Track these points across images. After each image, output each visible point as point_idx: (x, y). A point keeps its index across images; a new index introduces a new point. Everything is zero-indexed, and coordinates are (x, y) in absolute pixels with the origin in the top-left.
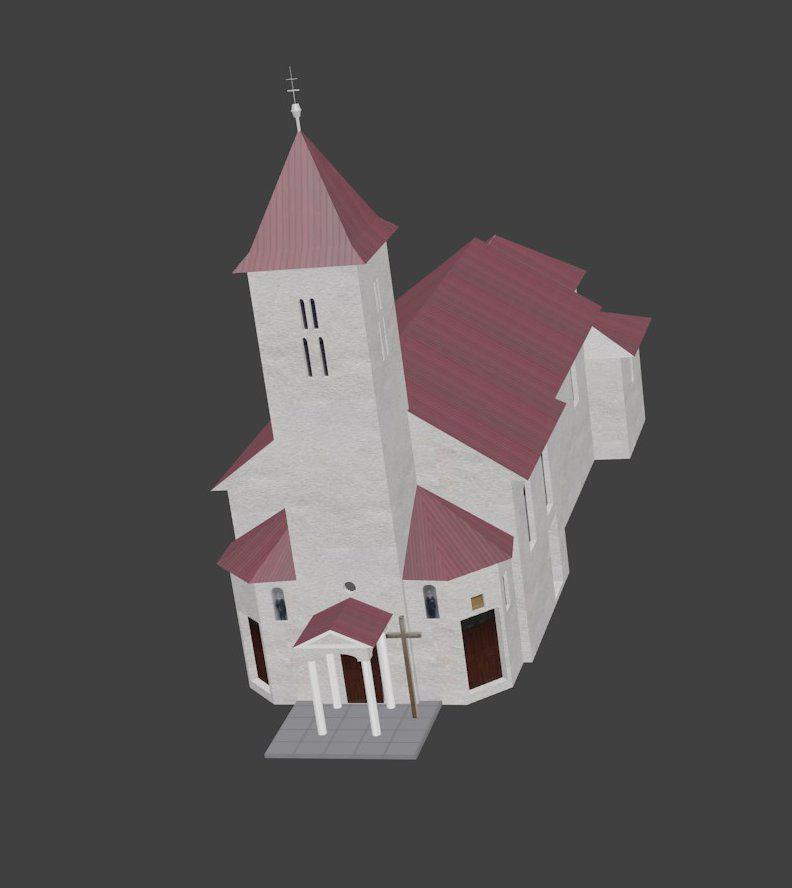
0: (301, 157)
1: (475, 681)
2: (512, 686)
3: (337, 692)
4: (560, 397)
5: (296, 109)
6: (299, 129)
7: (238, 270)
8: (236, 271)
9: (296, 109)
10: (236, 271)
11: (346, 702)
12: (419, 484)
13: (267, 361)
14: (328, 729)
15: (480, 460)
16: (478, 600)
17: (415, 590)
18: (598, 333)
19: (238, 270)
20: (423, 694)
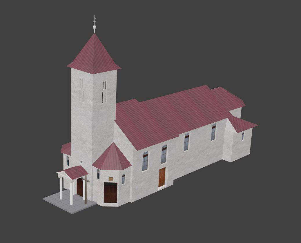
0: (93, 39)
1: (107, 199)
2: (131, 202)
3: (164, 187)
4: (179, 135)
5: (94, 27)
6: (94, 33)
7: (68, 66)
8: (68, 66)
9: (94, 27)
10: (68, 66)
11: (76, 193)
12: (117, 143)
13: (72, 93)
14: (63, 198)
15: (128, 141)
16: (111, 179)
17: (95, 169)
18: (252, 131)
19: (68, 66)
20: (89, 198)
